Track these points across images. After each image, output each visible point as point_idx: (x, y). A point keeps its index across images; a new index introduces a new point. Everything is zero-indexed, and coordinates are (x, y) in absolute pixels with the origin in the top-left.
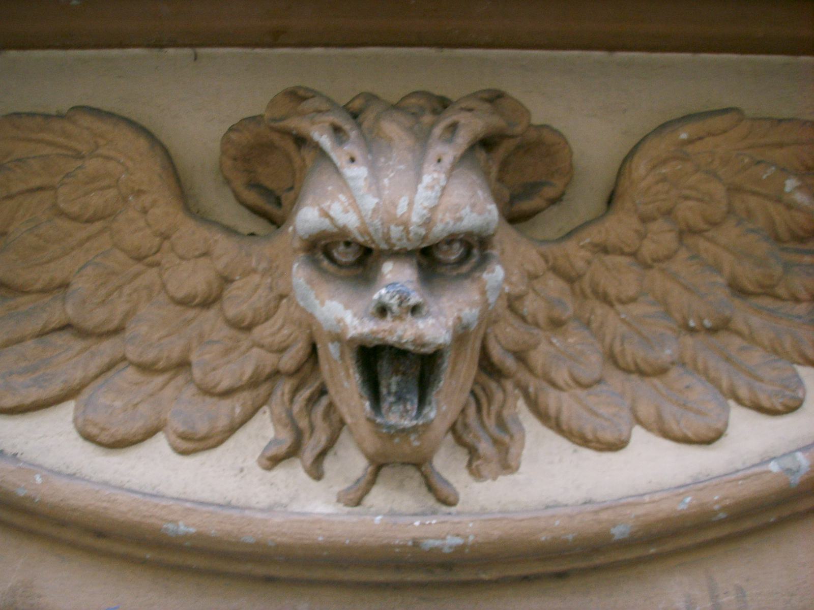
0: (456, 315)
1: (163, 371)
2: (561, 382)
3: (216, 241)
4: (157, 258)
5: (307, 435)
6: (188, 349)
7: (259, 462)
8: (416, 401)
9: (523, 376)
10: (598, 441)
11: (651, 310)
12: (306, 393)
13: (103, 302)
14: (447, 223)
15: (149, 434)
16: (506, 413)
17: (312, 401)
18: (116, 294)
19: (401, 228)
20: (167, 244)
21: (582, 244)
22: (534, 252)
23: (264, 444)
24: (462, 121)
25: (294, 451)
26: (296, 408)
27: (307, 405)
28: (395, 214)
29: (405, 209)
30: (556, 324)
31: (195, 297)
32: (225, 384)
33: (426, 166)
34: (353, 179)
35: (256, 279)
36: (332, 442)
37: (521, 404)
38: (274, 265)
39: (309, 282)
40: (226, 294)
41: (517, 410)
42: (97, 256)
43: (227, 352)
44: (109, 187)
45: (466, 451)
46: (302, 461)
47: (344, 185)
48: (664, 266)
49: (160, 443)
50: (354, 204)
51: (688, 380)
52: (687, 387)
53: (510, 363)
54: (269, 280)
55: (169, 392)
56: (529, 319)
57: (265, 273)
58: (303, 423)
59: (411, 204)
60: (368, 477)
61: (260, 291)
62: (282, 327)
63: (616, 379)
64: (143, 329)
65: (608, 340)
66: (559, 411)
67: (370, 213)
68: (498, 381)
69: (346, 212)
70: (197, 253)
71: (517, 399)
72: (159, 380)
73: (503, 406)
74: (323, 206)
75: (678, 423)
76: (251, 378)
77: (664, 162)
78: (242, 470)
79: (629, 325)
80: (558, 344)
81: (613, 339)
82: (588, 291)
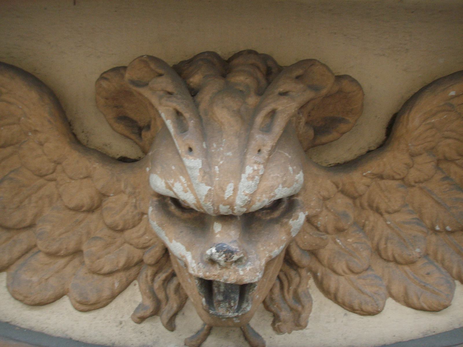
0: (267, 255)
1: (63, 256)
2: (340, 271)
3: (95, 168)
4: (54, 175)
5: (164, 303)
6: (80, 243)
7: (133, 317)
8: (237, 298)
9: (315, 265)
10: (362, 310)
11: (408, 217)
12: (162, 276)
13: (18, 207)
14: (264, 201)
15: (58, 297)
16: (300, 290)
17: (167, 280)
18: (26, 202)
19: (228, 207)
20: (59, 168)
21: (364, 174)
22: (329, 182)
23: (135, 306)
24: (280, 108)
25: (156, 312)
26: (156, 285)
27: (163, 284)
28: (224, 197)
29: (231, 193)
30: (339, 230)
31: (82, 207)
32: (107, 268)
33: (248, 156)
34: (191, 168)
35: (125, 198)
36: (181, 307)
37: (311, 282)
38: (137, 190)
39: (161, 225)
40: (105, 205)
41: (308, 286)
42: (11, 172)
43: (107, 245)
44: (14, 124)
45: (271, 314)
46: (161, 319)
47: (183, 170)
48: (422, 185)
49: (66, 303)
50: (191, 187)
51: (430, 268)
52: (428, 274)
53: (305, 260)
54: (134, 201)
55: (69, 269)
56: (321, 228)
57: (131, 195)
58: (161, 296)
59: (235, 190)
60: (205, 332)
61: (128, 208)
62: (144, 234)
63: (379, 267)
64: (48, 227)
65: (376, 239)
66: (337, 289)
67: (204, 197)
68: (296, 270)
69: (186, 192)
70: (82, 176)
71: (309, 278)
72: (62, 262)
73: (298, 286)
74: (168, 182)
75: (419, 299)
76: (124, 265)
77: (434, 115)
78: (121, 323)
79: (392, 229)
80: (340, 244)
81: (380, 239)
82: (366, 204)
